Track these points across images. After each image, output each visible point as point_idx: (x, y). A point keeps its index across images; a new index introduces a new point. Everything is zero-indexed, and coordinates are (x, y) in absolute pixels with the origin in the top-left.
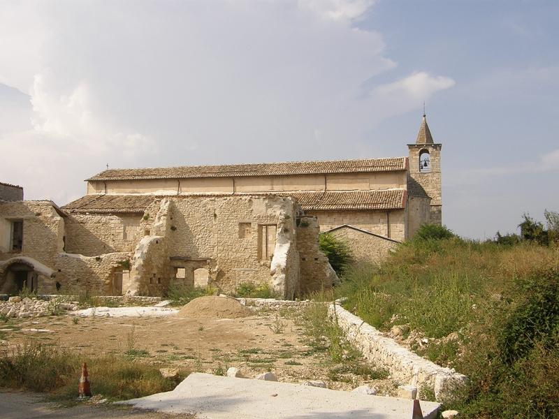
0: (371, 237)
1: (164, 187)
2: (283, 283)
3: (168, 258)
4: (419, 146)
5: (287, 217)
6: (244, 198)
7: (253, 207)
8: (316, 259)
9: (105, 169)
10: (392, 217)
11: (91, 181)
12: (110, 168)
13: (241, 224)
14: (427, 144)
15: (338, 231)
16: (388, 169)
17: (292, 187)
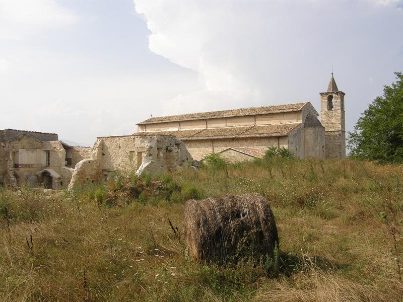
1: (172, 127)
4: (326, 94)
5: (151, 147)
9: (151, 117)
11: (139, 125)
12: (153, 117)
17: (237, 124)
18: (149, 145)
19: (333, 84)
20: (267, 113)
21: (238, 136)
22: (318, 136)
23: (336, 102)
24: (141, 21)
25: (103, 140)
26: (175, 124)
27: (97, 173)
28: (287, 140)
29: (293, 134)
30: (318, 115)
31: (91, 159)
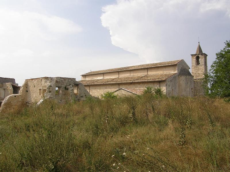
1: (100, 76)
4: (195, 55)
9: (90, 71)
11: (83, 76)
16: (170, 64)
17: (136, 74)
18: (49, 84)
19: (200, 49)
20: (155, 66)
21: (134, 81)
22: (188, 81)
23: (201, 60)
24: (106, 31)
26: (101, 75)
28: (165, 84)
29: (170, 80)
30: (190, 68)
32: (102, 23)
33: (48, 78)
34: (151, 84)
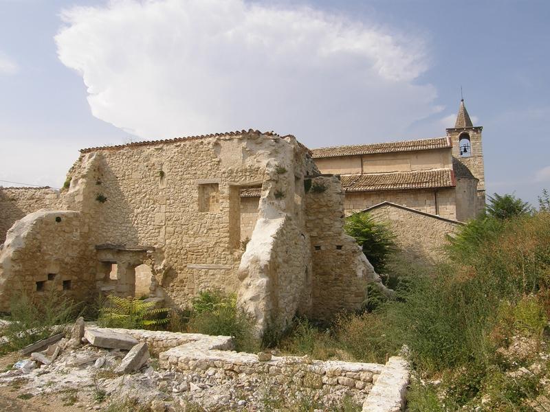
0: (422, 217)
2: (263, 295)
3: (92, 248)
4: (459, 130)
5: (281, 171)
6: (206, 141)
7: (221, 156)
8: (339, 247)
10: (440, 198)
13: (203, 187)
14: (466, 130)
15: (377, 211)
18: (274, 162)
24: (72, 81)
25: (101, 157)
27: (83, 258)
31: (63, 210)
32: (58, 55)
33: (258, 133)
34: (408, 196)
